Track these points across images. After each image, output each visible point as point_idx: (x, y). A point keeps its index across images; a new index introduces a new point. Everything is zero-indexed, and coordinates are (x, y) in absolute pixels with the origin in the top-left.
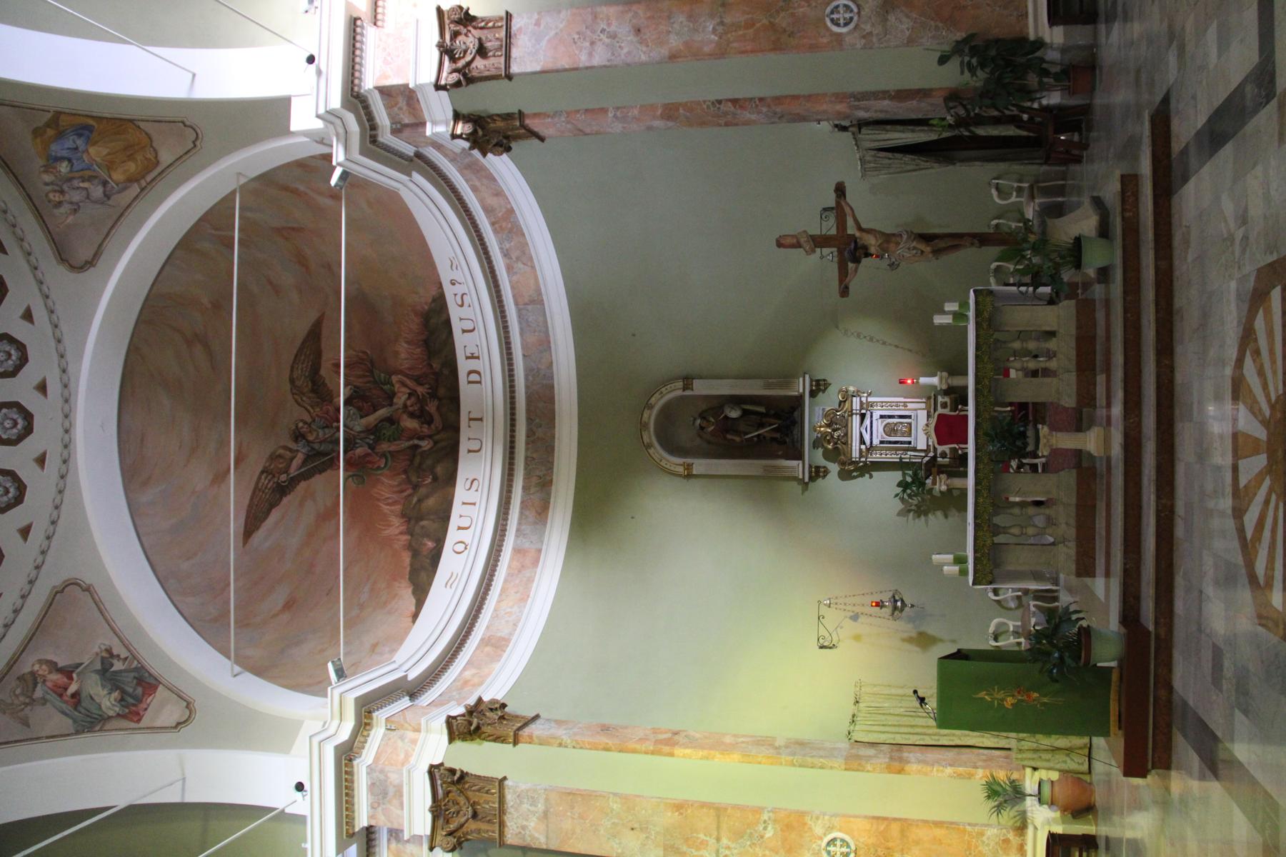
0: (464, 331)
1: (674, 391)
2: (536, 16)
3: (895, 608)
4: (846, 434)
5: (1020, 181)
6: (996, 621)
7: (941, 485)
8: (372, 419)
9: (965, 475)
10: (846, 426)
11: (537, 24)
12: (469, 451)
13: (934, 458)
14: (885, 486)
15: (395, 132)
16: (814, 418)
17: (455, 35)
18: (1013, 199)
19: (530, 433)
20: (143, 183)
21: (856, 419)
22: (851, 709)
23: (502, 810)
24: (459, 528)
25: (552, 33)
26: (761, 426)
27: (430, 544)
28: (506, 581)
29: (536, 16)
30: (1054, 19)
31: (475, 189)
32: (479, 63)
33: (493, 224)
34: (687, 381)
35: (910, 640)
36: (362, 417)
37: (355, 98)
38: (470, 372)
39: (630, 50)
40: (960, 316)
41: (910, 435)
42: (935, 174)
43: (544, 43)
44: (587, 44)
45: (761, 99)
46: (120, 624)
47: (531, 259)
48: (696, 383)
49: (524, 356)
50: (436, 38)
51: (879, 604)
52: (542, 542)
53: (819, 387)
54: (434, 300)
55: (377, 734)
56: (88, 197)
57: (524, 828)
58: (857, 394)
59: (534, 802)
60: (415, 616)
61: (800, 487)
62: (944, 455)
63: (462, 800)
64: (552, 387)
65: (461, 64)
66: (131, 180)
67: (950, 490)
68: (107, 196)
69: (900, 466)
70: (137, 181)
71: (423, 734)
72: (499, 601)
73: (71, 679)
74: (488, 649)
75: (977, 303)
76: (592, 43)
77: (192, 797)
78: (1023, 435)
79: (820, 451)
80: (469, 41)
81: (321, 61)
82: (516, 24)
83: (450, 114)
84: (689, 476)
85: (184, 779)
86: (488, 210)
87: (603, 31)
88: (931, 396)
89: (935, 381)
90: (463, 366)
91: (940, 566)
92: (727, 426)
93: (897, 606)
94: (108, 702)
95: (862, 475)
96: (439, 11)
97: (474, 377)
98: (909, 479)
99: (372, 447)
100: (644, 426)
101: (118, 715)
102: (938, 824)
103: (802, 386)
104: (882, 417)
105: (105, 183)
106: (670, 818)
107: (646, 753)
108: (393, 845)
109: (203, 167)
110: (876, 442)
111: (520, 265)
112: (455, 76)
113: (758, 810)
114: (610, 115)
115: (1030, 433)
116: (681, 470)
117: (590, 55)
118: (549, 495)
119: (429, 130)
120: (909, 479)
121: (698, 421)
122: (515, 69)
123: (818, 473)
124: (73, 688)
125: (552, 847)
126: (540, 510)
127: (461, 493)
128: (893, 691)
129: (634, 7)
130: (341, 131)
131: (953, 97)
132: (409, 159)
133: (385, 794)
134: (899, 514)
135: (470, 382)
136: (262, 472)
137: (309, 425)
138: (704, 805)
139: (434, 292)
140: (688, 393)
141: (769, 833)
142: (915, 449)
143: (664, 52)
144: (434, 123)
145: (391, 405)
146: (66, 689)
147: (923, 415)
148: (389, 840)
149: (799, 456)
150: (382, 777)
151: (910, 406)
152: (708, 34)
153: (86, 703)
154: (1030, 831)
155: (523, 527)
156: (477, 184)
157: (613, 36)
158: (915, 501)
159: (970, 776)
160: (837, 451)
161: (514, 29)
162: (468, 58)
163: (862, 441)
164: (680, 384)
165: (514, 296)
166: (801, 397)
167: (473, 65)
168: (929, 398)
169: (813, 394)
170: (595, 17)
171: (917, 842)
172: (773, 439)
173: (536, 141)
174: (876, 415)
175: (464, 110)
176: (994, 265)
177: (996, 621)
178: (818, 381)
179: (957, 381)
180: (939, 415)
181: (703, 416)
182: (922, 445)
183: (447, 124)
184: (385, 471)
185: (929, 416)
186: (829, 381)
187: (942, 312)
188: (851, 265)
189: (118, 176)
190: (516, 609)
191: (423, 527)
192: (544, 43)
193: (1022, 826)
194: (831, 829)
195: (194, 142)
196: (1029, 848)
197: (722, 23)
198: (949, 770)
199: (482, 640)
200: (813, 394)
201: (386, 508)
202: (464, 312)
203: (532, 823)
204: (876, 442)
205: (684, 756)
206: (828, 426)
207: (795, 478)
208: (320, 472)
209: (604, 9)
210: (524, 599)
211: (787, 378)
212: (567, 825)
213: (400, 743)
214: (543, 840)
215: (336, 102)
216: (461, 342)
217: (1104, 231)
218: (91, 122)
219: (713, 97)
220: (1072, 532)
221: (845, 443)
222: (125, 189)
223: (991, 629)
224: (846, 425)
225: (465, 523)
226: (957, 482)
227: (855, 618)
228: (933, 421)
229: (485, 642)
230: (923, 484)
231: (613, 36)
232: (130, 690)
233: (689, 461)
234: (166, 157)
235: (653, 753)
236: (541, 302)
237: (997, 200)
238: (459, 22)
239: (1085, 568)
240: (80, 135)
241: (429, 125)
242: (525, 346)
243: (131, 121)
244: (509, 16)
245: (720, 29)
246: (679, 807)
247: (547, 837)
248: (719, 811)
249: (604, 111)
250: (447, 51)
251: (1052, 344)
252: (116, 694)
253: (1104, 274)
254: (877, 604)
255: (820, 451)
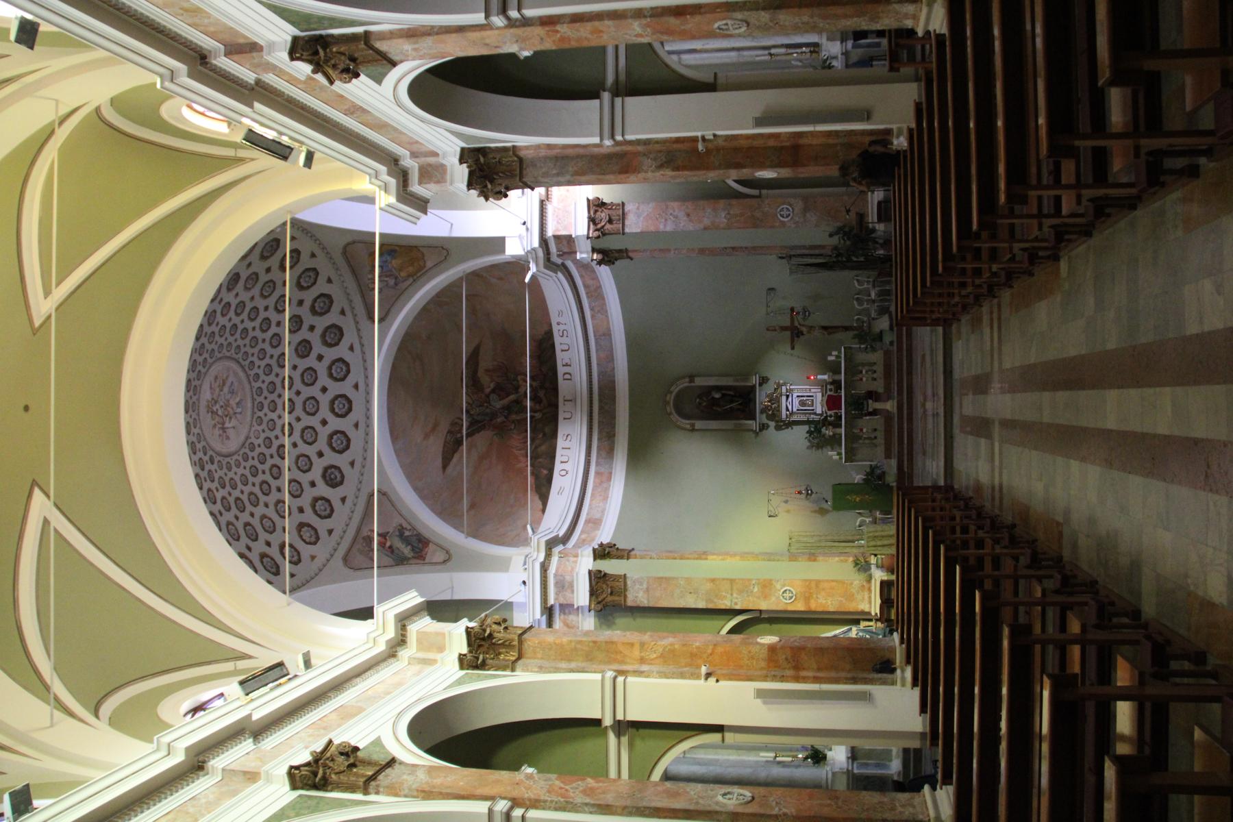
0: (562, 351)
1: (685, 383)
2: (637, 205)
3: (808, 494)
4: (779, 406)
5: (868, 278)
6: (859, 520)
7: (828, 432)
8: (506, 401)
9: (841, 427)
10: (779, 402)
11: (638, 208)
12: (565, 419)
13: (826, 417)
14: (800, 432)
15: (559, 256)
16: (761, 398)
17: (596, 211)
18: (865, 286)
19: (601, 408)
20: (415, 277)
21: (784, 398)
22: (788, 541)
23: (625, 589)
24: (562, 462)
25: (646, 214)
26: (732, 402)
27: (545, 472)
28: (593, 490)
29: (637, 205)
30: (880, 220)
31: (581, 276)
32: (608, 226)
33: (587, 293)
34: (692, 378)
35: (815, 512)
36: (500, 400)
37: (544, 241)
38: (565, 374)
39: (685, 224)
40: (838, 357)
41: (813, 406)
42: (825, 275)
43: (642, 219)
44: (663, 220)
45: (746, 248)
46: (404, 512)
47: (607, 311)
48: (696, 379)
49: (598, 364)
50: (586, 214)
51: (800, 493)
52: (612, 468)
53: (764, 381)
54: (546, 333)
55: (555, 560)
56: (387, 285)
57: (636, 597)
58: (785, 384)
59: (641, 584)
60: (543, 511)
61: (754, 435)
62: (831, 416)
63: (604, 586)
64: (614, 382)
65: (599, 226)
66: (409, 276)
67: (834, 435)
68: (396, 284)
69: (808, 422)
70: (412, 276)
71: (579, 558)
72: (591, 500)
73: (386, 539)
74: (590, 525)
75: (845, 352)
76: (666, 220)
77: (457, 597)
78: (862, 403)
79: (764, 415)
80: (603, 215)
81: (529, 224)
82: (627, 208)
83: (590, 249)
84: (693, 430)
85: (453, 587)
86: (586, 286)
87: (671, 214)
88: (823, 385)
89: (826, 377)
90: (561, 370)
91: (832, 456)
92: (714, 402)
93: (809, 493)
94: (407, 551)
95: (787, 428)
96: (588, 200)
97: (567, 376)
98: (812, 429)
99: (506, 417)
100: (666, 403)
101: (413, 557)
102: (833, 581)
103: (755, 380)
104: (798, 396)
105: (396, 278)
106: (709, 586)
107: (694, 559)
108: (562, 617)
109: (447, 269)
110: (795, 410)
111: (599, 315)
112: (597, 233)
113: (750, 580)
114: (672, 252)
115: (865, 403)
116: (688, 427)
117: (665, 225)
118: (613, 442)
119: (578, 256)
120: (812, 429)
121: (698, 400)
122: (627, 230)
123: (764, 427)
124: (388, 544)
125: (651, 605)
126: (608, 451)
127: (561, 442)
128: (808, 534)
129: (686, 204)
130: (534, 256)
131: (835, 248)
132: (557, 265)
133: (563, 587)
134: (808, 448)
135: (564, 379)
136: (448, 433)
137: (471, 405)
138: (724, 579)
139: (546, 328)
140: (693, 384)
141: (756, 590)
142: (815, 414)
143: (702, 226)
144: (581, 253)
145: (517, 392)
146: (385, 544)
147: (819, 395)
148: (560, 615)
149: (754, 418)
150: (562, 578)
151: (813, 390)
152: (722, 218)
153: (396, 551)
154: (873, 581)
155: (600, 460)
156: (584, 274)
157: (676, 217)
158: (816, 441)
159: (846, 561)
160: (774, 415)
161: (626, 210)
162: (603, 224)
163: (787, 409)
164: (687, 380)
165: (594, 332)
166: (754, 386)
167: (605, 228)
168: (823, 386)
169: (761, 385)
170: (667, 207)
171: (823, 589)
172: (739, 409)
173: (629, 260)
174: (795, 395)
175: (597, 247)
176: (856, 317)
177: (859, 520)
178: (763, 378)
179: (836, 377)
180: (829, 396)
181: (700, 396)
182: (819, 411)
183: (587, 253)
184: (515, 431)
185: (823, 396)
186: (769, 376)
187: (831, 355)
188: (796, 338)
189: (403, 274)
190: (601, 504)
191: (540, 462)
192: (642, 219)
193: (870, 578)
194: (784, 586)
195: (446, 257)
196: (873, 588)
197: (729, 214)
198: (837, 559)
199: (586, 521)
200: (761, 385)
201: (517, 452)
202: (564, 340)
203: (641, 594)
204: (795, 410)
205: (712, 559)
206: (769, 401)
207: (752, 430)
208: (478, 432)
209: (672, 204)
210: (606, 498)
211: (746, 376)
212: (658, 594)
213: (567, 563)
214: (646, 602)
215: (536, 244)
216: (561, 357)
217: (891, 328)
218: (397, 248)
219: (723, 246)
220: (883, 442)
221: (778, 411)
222: (406, 280)
223: (858, 524)
224: (778, 401)
225: (565, 459)
226: (838, 430)
227: (786, 502)
228: (825, 398)
229: (588, 521)
230: (820, 432)
231: (676, 217)
232: (416, 545)
233: (693, 422)
234: (429, 264)
235: (697, 559)
236: (610, 335)
237: (857, 306)
238: (598, 206)
239: (888, 455)
240: (389, 255)
241: (578, 254)
242: (598, 358)
243: (416, 247)
244: (623, 204)
245: (728, 217)
246: (713, 580)
247: (648, 601)
248: (732, 581)
249: (669, 250)
250: (592, 220)
251: (874, 368)
252: (409, 547)
253: (891, 343)
254: (799, 493)
255: (764, 415)
